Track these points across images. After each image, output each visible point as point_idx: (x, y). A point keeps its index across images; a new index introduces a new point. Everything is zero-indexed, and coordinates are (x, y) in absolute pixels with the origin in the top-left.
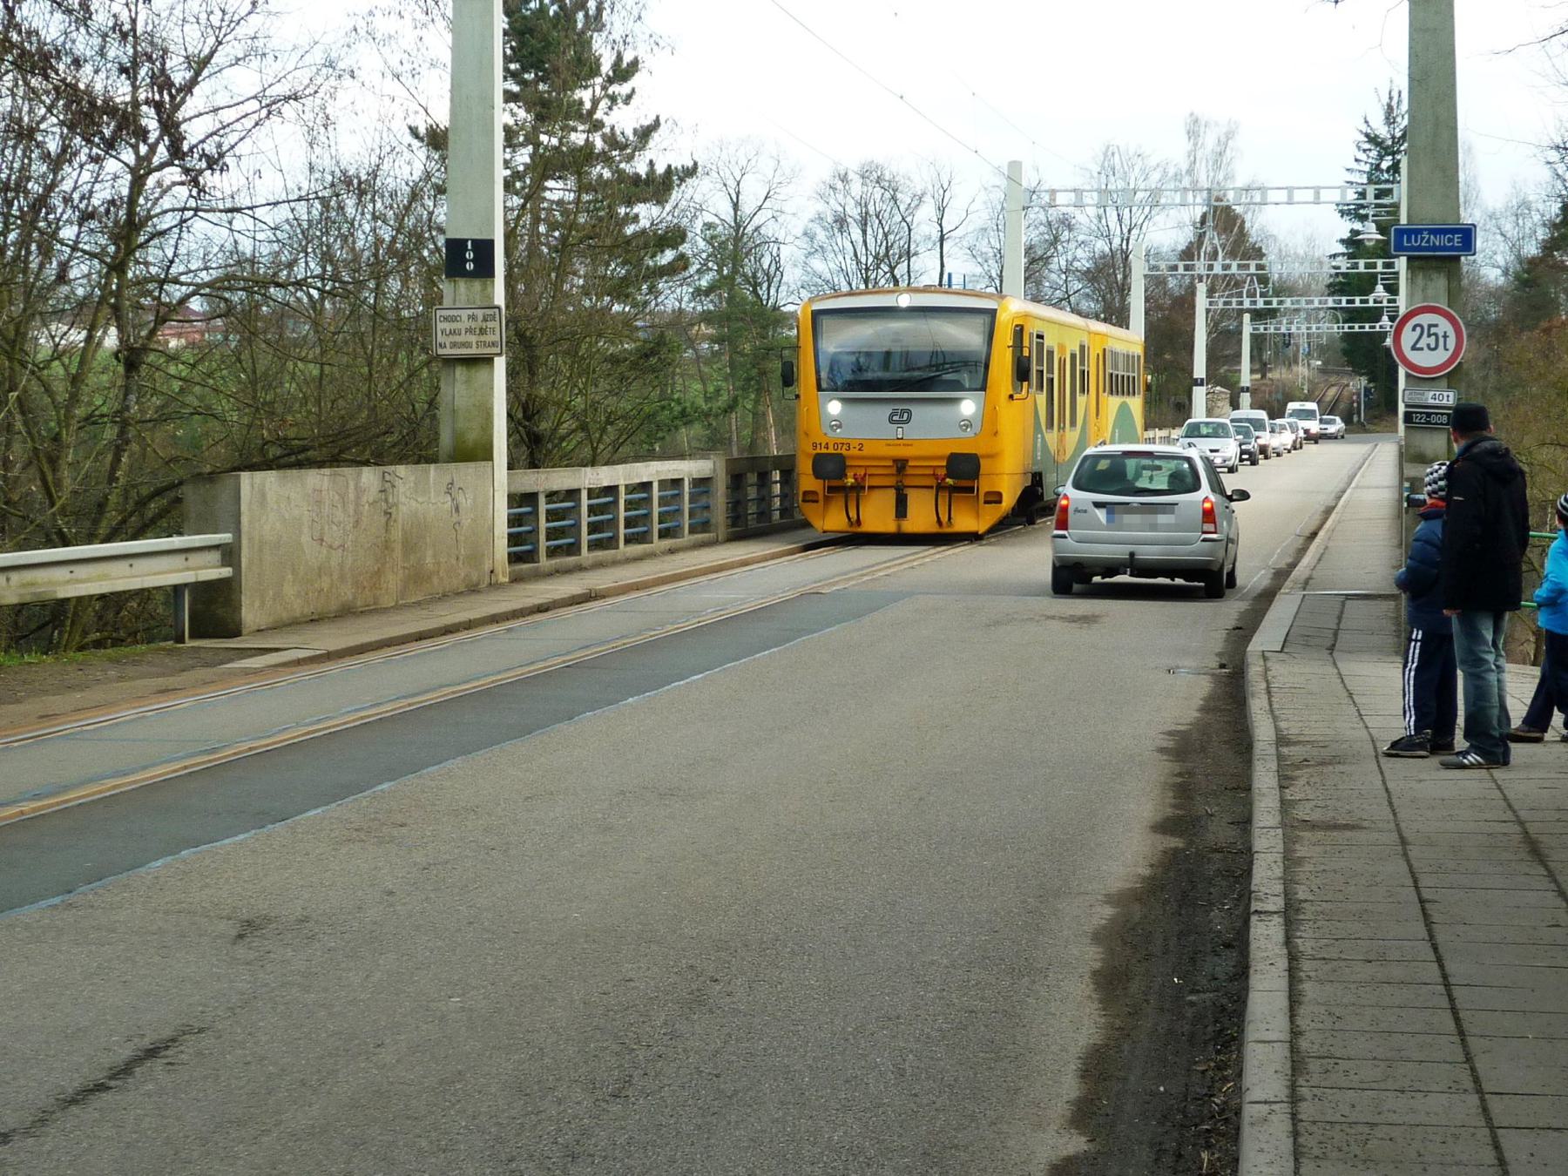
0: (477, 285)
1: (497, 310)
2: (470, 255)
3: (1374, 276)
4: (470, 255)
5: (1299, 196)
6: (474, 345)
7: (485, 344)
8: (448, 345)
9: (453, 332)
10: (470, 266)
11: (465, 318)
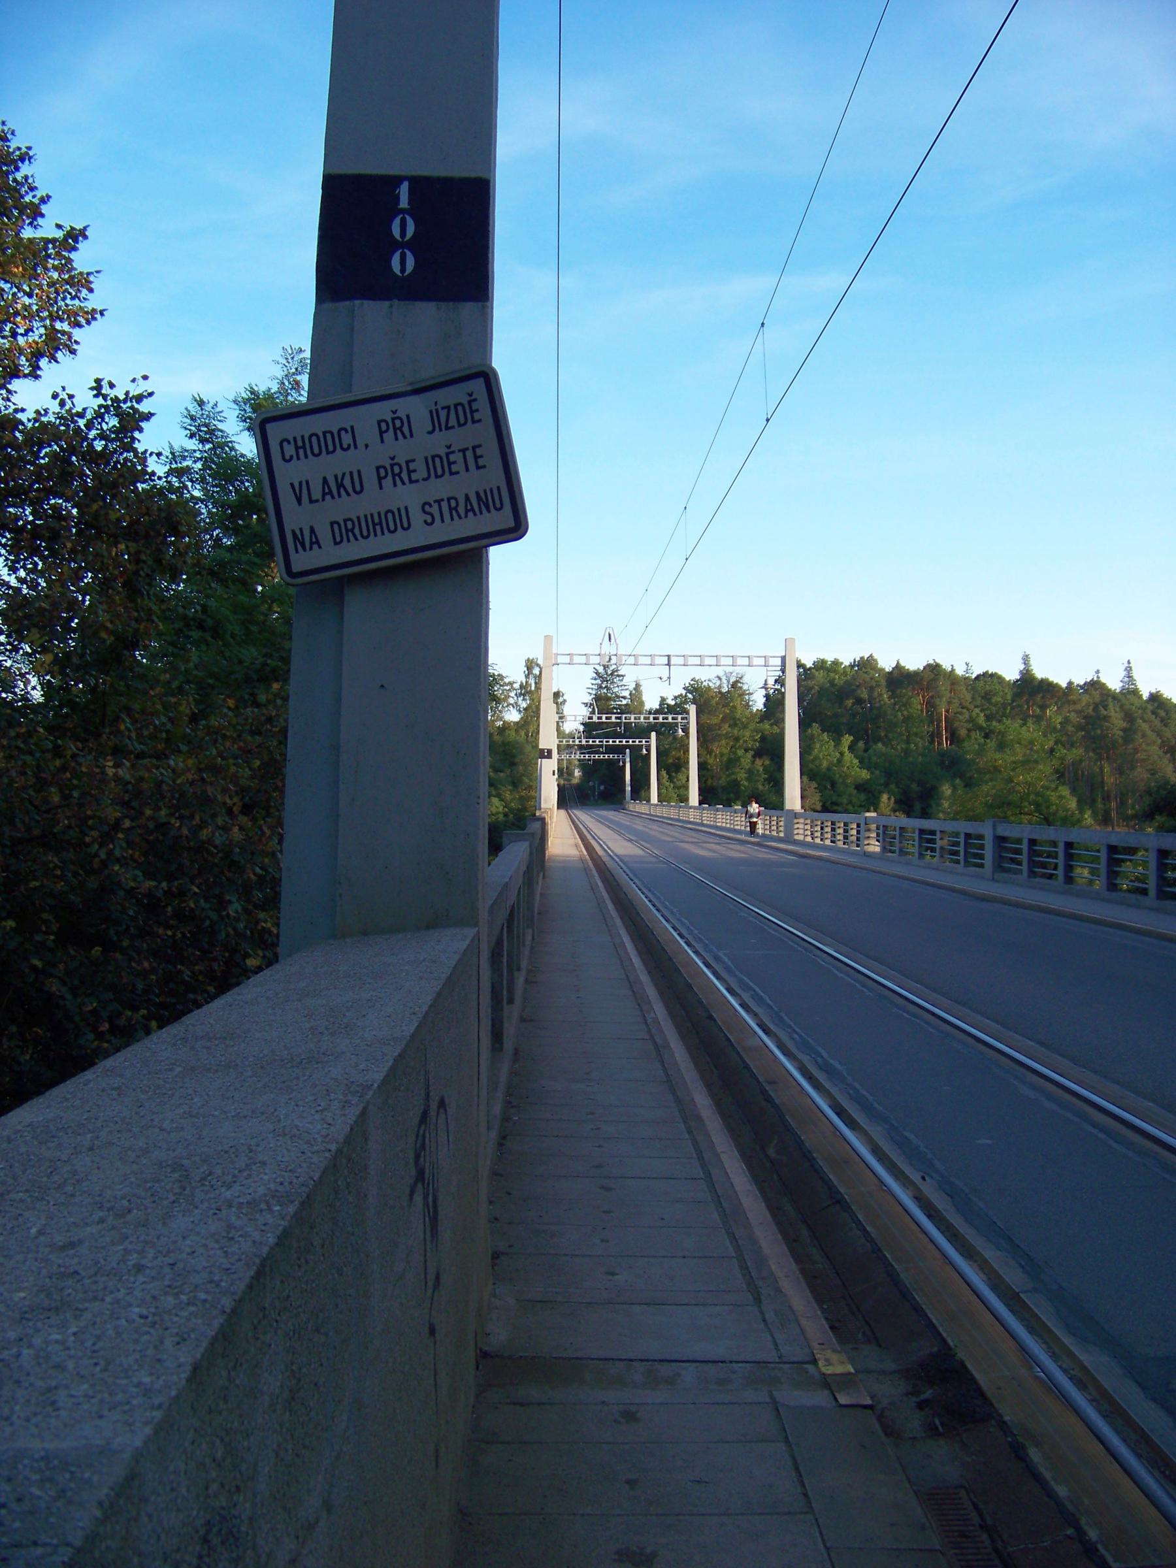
0: (427, 313)
1: (478, 385)
2: (403, 228)
3: (677, 723)
4: (403, 228)
5: (576, 659)
6: (417, 517)
7: (454, 508)
8: (324, 534)
9: (334, 488)
10: (402, 264)
11: (367, 432)
